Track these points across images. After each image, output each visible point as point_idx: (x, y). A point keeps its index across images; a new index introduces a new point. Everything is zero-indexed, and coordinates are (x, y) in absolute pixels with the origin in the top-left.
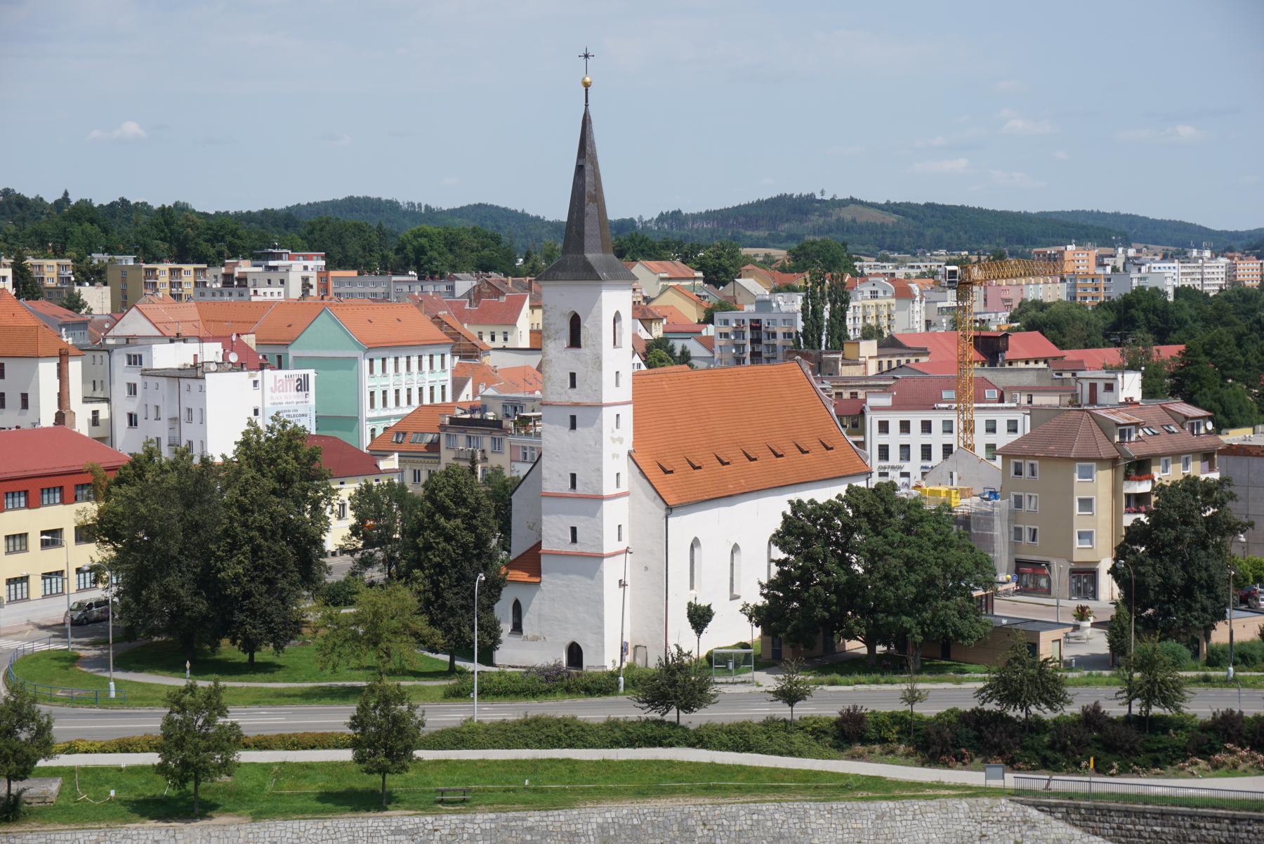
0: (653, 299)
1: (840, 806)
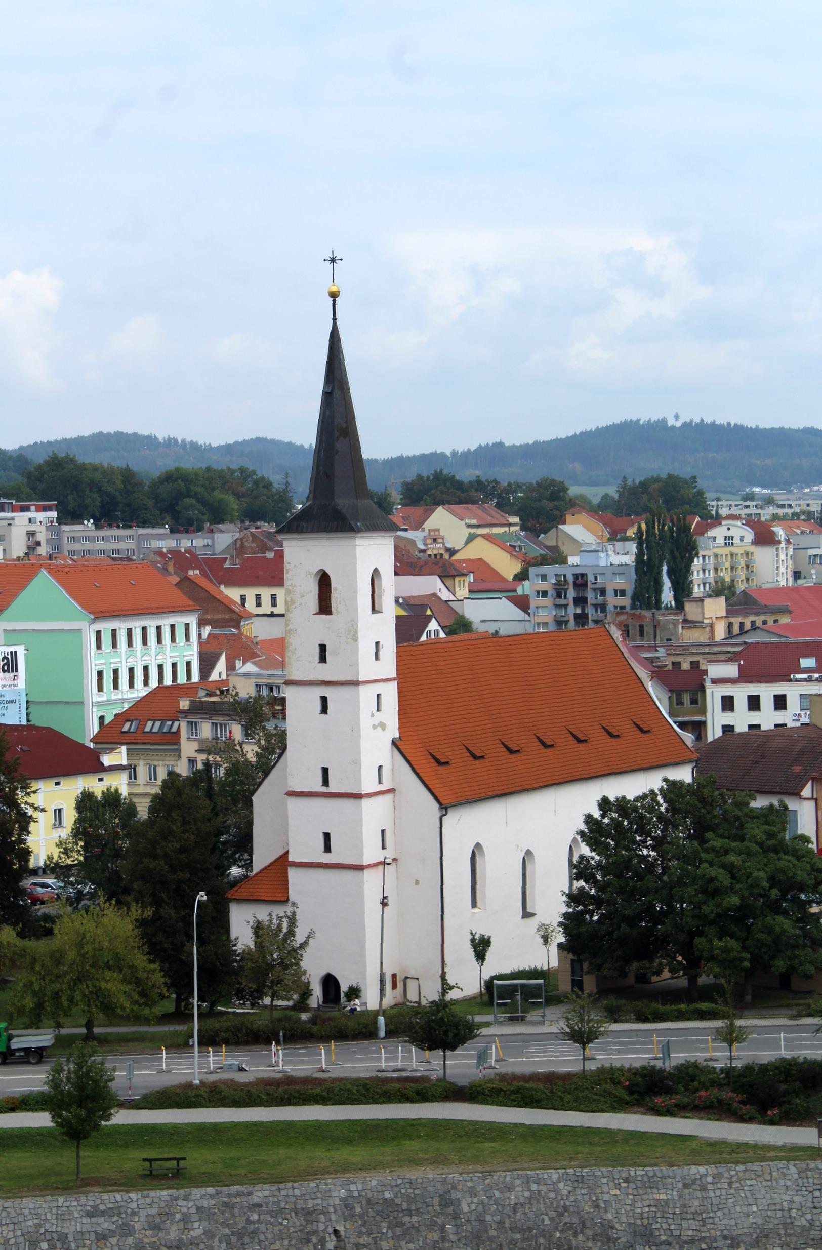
0: (456, 552)
1: (639, 1173)
